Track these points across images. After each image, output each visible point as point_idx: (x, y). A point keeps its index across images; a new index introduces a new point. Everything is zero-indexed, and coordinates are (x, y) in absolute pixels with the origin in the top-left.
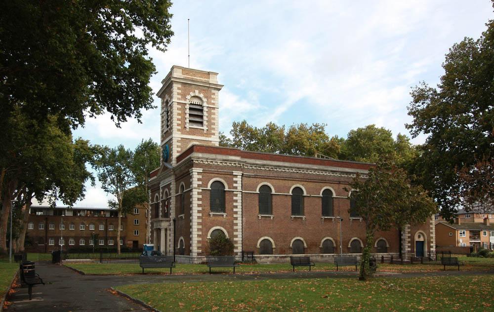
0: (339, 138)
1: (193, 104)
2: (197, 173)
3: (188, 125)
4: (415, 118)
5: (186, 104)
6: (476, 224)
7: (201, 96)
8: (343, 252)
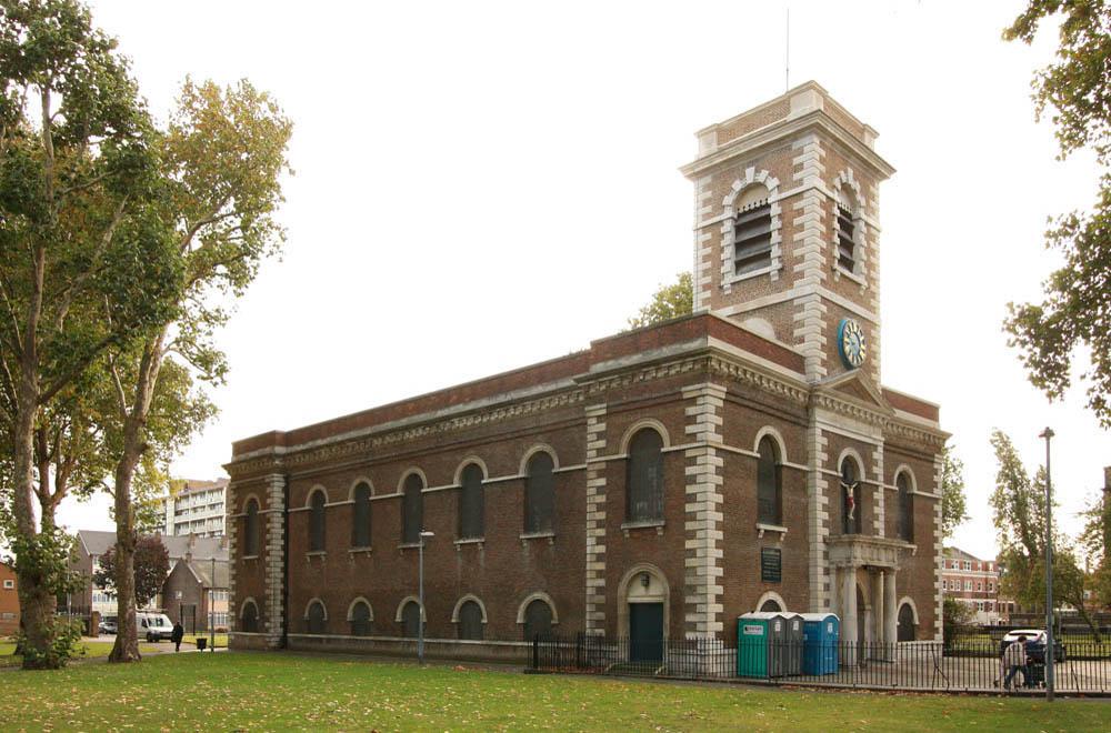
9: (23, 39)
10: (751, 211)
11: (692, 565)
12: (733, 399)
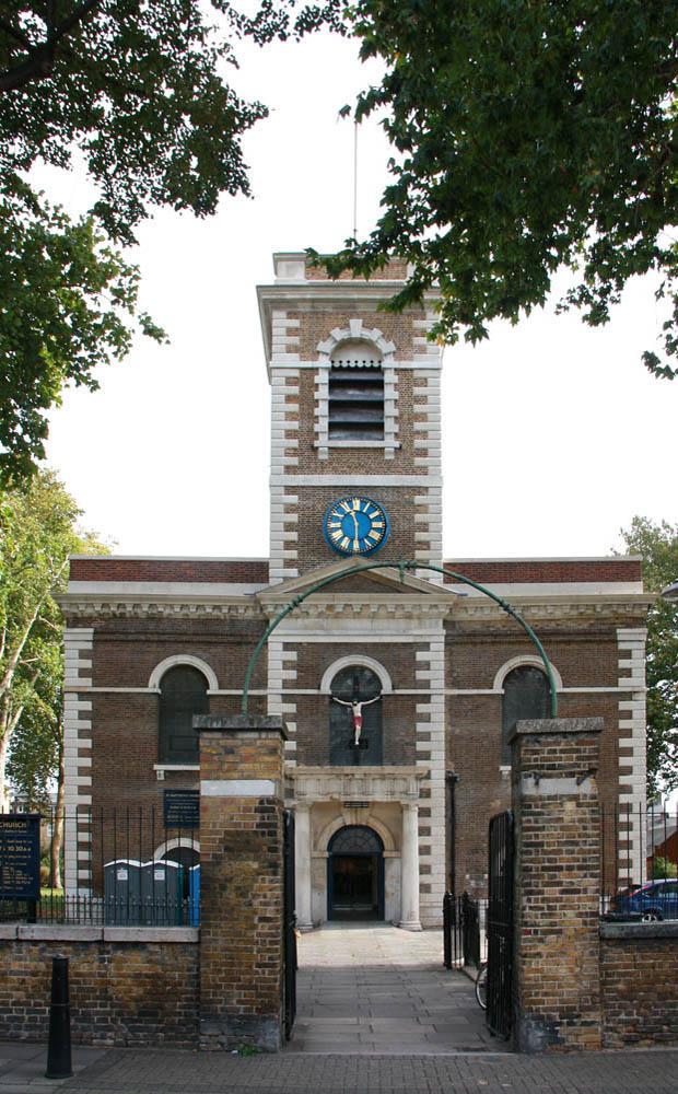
0: (601, 324)
1: (341, 369)
2: (76, 696)
3: (323, 442)
4: (655, 245)
5: (317, 369)
6: (621, 650)
7: (374, 335)
8: (401, 658)
9: (540, 1034)
10: (349, 369)
11: (420, 464)
12: (353, 394)
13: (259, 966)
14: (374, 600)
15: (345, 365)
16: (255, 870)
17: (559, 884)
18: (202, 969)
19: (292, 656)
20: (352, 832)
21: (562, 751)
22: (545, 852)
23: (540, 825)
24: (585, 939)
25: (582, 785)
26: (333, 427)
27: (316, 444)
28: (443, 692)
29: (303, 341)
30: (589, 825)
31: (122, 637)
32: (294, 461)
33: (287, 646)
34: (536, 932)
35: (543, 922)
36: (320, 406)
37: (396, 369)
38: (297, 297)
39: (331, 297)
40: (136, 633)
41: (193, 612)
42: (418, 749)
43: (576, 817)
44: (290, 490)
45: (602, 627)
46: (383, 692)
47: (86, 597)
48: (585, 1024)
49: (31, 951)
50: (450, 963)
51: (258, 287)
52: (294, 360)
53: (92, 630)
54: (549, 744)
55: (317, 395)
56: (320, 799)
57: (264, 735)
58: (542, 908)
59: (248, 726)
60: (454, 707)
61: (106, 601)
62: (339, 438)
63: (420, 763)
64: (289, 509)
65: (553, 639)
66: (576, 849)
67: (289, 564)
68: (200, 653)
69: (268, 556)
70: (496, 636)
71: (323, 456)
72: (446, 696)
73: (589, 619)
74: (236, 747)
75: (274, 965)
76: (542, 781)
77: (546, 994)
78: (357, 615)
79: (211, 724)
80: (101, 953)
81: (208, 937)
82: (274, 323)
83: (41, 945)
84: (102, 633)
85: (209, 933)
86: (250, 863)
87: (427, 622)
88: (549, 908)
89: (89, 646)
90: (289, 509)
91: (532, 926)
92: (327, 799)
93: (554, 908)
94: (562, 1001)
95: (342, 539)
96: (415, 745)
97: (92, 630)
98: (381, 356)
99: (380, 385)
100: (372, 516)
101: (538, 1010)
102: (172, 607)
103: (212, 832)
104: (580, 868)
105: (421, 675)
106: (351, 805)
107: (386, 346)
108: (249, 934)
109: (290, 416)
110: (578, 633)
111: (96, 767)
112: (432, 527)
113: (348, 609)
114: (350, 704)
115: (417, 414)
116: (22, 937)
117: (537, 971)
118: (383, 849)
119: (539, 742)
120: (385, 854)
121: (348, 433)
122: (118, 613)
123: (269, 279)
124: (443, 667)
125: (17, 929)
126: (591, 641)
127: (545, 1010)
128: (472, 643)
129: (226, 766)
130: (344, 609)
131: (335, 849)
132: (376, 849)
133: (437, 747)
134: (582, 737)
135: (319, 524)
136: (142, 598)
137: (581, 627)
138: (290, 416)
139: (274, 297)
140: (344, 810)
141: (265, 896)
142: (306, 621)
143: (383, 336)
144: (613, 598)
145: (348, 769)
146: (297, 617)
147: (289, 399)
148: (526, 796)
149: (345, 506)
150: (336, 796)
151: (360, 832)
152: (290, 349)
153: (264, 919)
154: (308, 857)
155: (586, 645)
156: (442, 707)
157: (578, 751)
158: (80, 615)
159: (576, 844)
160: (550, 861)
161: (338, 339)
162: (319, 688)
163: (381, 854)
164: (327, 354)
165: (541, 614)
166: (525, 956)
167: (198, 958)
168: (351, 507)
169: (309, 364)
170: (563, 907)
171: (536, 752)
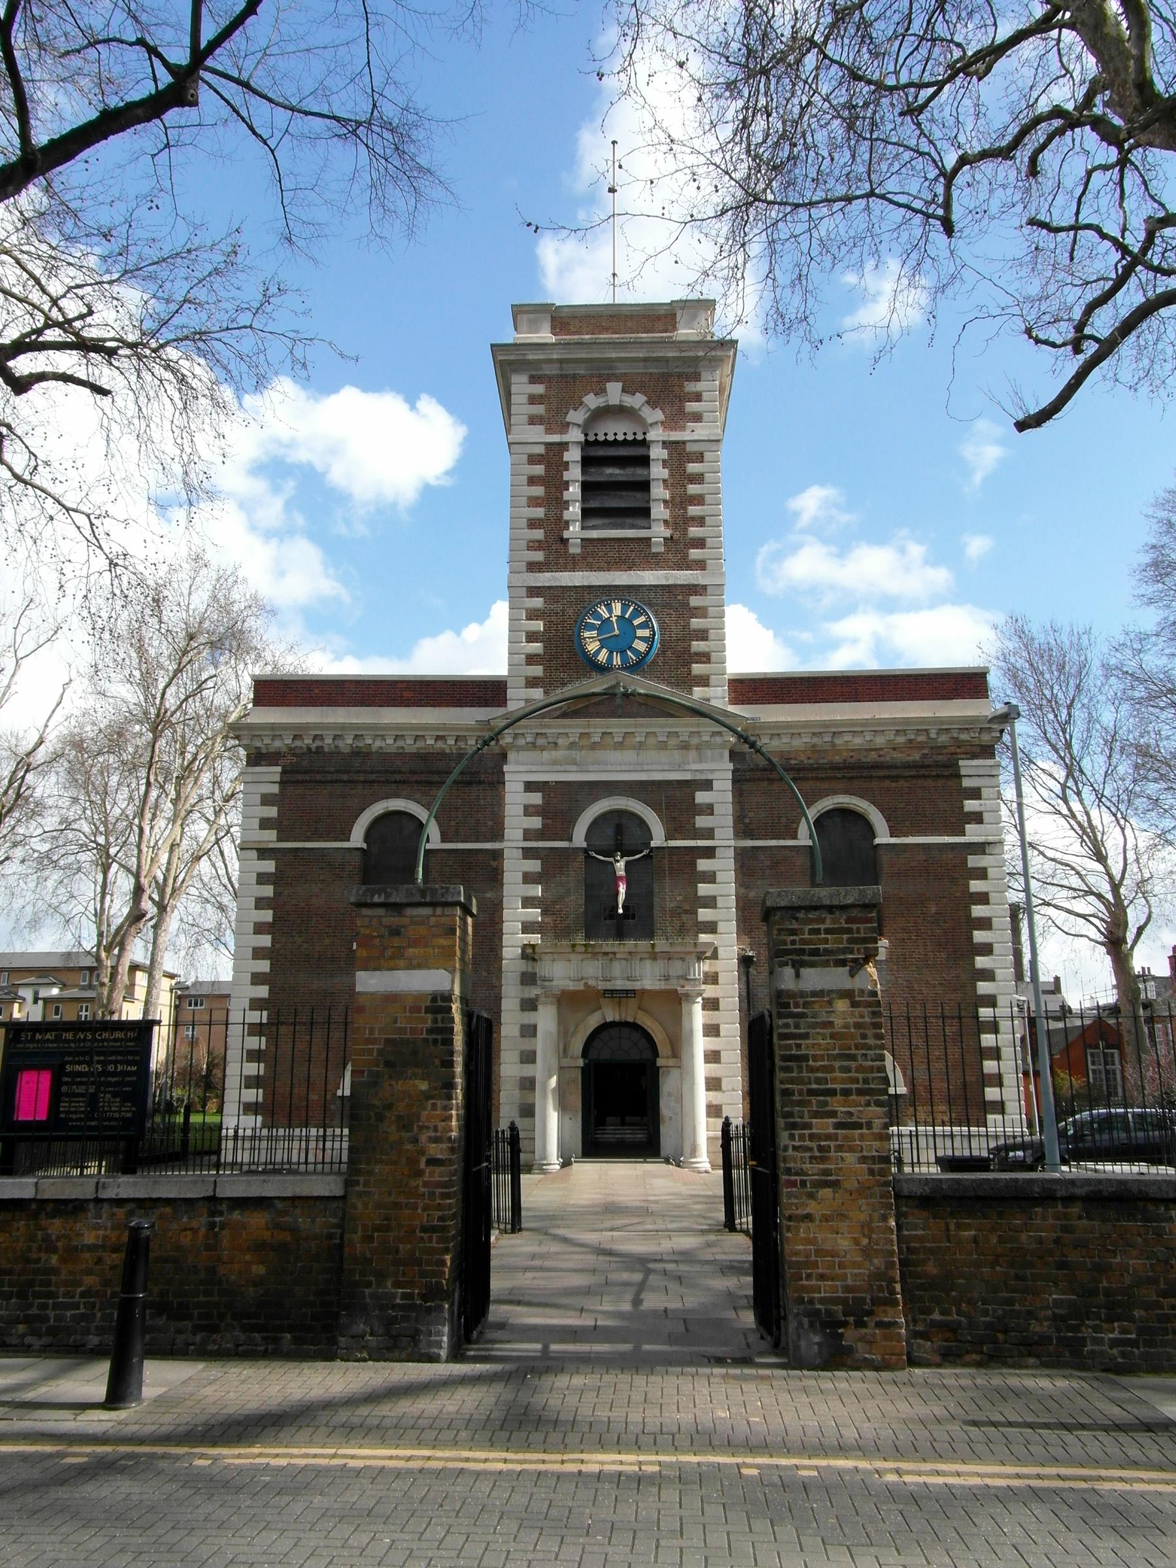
1: (596, 442)
3: (574, 531)
5: (567, 443)
6: (966, 788)
10: (606, 443)
12: (613, 473)
13: (424, 1229)
14: (641, 727)
15: (601, 438)
16: (423, 1092)
17: (833, 1114)
18: (347, 1236)
19: (536, 798)
20: (614, 1032)
21: (827, 931)
22: (812, 1070)
23: (802, 1031)
24: (872, 1196)
25: (857, 977)
26: (586, 513)
27: (566, 535)
28: (732, 843)
29: (548, 410)
30: (869, 1032)
31: (318, 777)
32: (539, 556)
33: (530, 787)
34: (803, 1183)
35: (813, 1168)
36: (571, 489)
37: (664, 442)
38: (542, 357)
39: (584, 356)
40: (338, 771)
41: (409, 745)
42: (700, 919)
43: (851, 1021)
44: (533, 592)
45: (940, 758)
46: (653, 844)
47: (273, 727)
48: (880, 1325)
49: (114, 1214)
50: (733, 1220)
51: (492, 346)
52: (538, 435)
53: (279, 769)
54: (811, 921)
55: (566, 476)
56: (572, 986)
57: (439, 911)
58: (810, 1149)
59: (417, 899)
60: (746, 862)
61: (298, 732)
62: (594, 528)
63: (704, 938)
64: (532, 615)
65: (874, 773)
66: (853, 1064)
67: (532, 683)
68: (418, 796)
69: (506, 673)
70: (799, 770)
71: (575, 549)
72: (735, 848)
73: (923, 748)
74: (403, 927)
75: (444, 1229)
76: (803, 971)
77: (822, 1277)
78: (620, 746)
79: (372, 896)
80: (212, 1214)
81: (357, 1188)
82: (514, 389)
83: (129, 1206)
84: (292, 772)
85: (357, 1183)
86: (417, 1082)
87: (709, 753)
88: (821, 1149)
89: (275, 789)
90: (532, 615)
91: (797, 1174)
92: (580, 987)
93: (827, 1149)
94: (847, 1289)
95: (598, 651)
96: (696, 914)
97: (279, 769)
98: (646, 426)
99: (645, 461)
100: (636, 622)
101: (811, 1301)
102: (383, 738)
103: (368, 1041)
104: (860, 1092)
105: (701, 822)
106: (612, 994)
107: (654, 415)
108: (413, 1183)
109: (533, 502)
110: (907, 766)
111: (277, 946)
112: (712, 634)
113: (608, 739)
114: (611, 859)
115: (691, 496)
116: (104, 1195)
117: (808, 1241)
118: (656, 1054)
119: (797, 919)
120: (660, 1062)
121: (607, 521)
122: (314, 746)
123: (510, 336)
124: (731, 812)
125: (97, 1183)
126: (925, 777)
127: (823, 1301)
128: (768, 779)
129: (389, 952)
130: (456, 741)
131: (593, 1054)
132: (648, 1055)
133: (726, 915)
134: (855, 913)
135: (570, 632)
136: (343, 727)
137: (910, 759)
138: (533, 502)
139: (512, 358)
140: (604, 1002)
141: (436, 1129)
142: (554, 753)
143: (648, 402)
144: (951, 720)
145: (610, 945)
146: (542, 749)
147: (532, 480)
148: (782, 991)
149: (603, 611)
150: (592, 983)
151: (625, 1032)
152: (533, 420)
153: (433, 1162)
154: (556, 1066)
155: (920, 782)
156: (731, 863)
157: (849, 931)
158: (264, 751)
159: (853, 1058)
160: (818, 1081)
161: (593, 407)
162: (570, 840)
163: (655, 1062)
164: (579, 426)
165: (858, 741)
166: (790, 1218)
167: (343, 1219)
168: (610, 611)
169: (555, 438)
170: (839, 1148)
171: (793, 932)
